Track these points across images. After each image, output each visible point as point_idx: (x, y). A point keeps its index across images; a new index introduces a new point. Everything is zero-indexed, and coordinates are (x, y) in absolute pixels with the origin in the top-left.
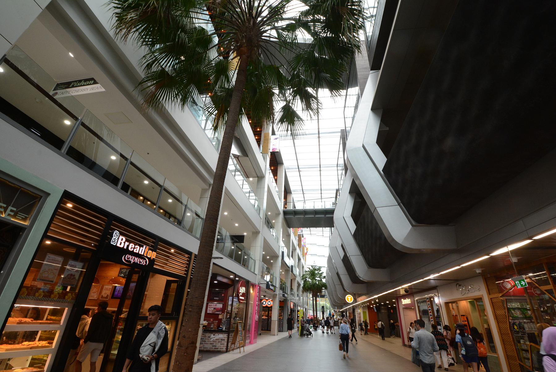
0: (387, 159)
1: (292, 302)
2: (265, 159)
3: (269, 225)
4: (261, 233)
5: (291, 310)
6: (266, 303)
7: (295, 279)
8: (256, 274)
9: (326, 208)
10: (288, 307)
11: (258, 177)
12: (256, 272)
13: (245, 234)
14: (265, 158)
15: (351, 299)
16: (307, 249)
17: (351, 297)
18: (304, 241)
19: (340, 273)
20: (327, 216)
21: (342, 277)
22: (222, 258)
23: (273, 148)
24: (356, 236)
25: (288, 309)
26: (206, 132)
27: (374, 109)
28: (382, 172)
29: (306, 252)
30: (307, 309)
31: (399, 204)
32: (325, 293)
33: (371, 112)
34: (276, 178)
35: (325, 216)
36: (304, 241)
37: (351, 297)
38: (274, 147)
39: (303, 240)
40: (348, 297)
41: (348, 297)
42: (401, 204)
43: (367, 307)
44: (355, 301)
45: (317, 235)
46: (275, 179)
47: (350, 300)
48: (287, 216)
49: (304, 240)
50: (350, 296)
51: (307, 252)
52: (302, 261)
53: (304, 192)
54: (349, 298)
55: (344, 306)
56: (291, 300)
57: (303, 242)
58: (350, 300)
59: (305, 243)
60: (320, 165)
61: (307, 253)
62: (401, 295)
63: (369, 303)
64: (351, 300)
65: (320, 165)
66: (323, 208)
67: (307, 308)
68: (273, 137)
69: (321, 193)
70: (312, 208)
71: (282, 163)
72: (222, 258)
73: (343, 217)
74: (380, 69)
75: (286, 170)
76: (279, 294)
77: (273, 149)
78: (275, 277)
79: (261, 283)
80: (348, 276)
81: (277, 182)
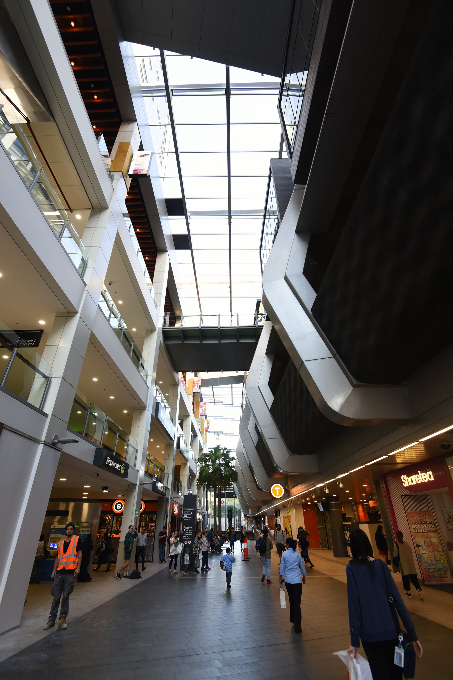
0: (317, 295)
1: (176, 503)
2: (158, 307)
3: (131, 347)
4: (147, 408)
5: (174, 517)
6: (122, 506)
7: (185, 464)
8: (46, 415)
9: (240, 325)
10: (166, 512)
11: (93, 208)
12: (49, 408)
13: (42, 322)
14: (158, 304)
15: (280, 490)
16: (208, 423)
17: (279, 488)
18: (203, 408)
19: (253, 466)
20: (241, 341)
21: (255, 470)
22: (76, 442)
23: (137, 168)
24: (273, 410)
25: (167, 516)
26: (63, 241)
27: (298, 231)
28: (311, 313)
29: (207, 427)
30: (206, 517)
31: (334, 356)
32: (233, 490)
33: (295, 234)
34: (184, 374)
35: (238, 341)
36: (203, 408)
37: (279, 488)
38: (138, 167)
39: (202, 406)
40: (275, 488)
41: (275, 488)
42: (337, 355)
43: (301, 506)
44: (287, 493)
45: (224, 403)
46: (183, 375)
47: (278, 494)
48: (170, 342)
49: (204, 405)
50: (278, 486)
51: (208, 427)
52: (199, 437)
53: (215, 396)
54: (277, 489)
55: (264, 507)
56: (173, 499)
57: (202, 409)
58: (278, 494)
59: (205, 410)
60: (230, 218)
61: (207, 429)
62: (400, 466)
63: (343, 484)
64: (280, 494)
65: (230, 218)
66: (234, 324)
67: (206, 514)
68: (201, 403)
69: (232, 398)
70: (217, 325)
71: (132, 119)
72: (76, 442)
73: (258, 386)
74: (306, 184)
75: (203, 397)
76: (171, 498)
77: (134, 171)
78: (166, 474)
79: (145, 482)
80: (263, 469)
81: (153, 273)
